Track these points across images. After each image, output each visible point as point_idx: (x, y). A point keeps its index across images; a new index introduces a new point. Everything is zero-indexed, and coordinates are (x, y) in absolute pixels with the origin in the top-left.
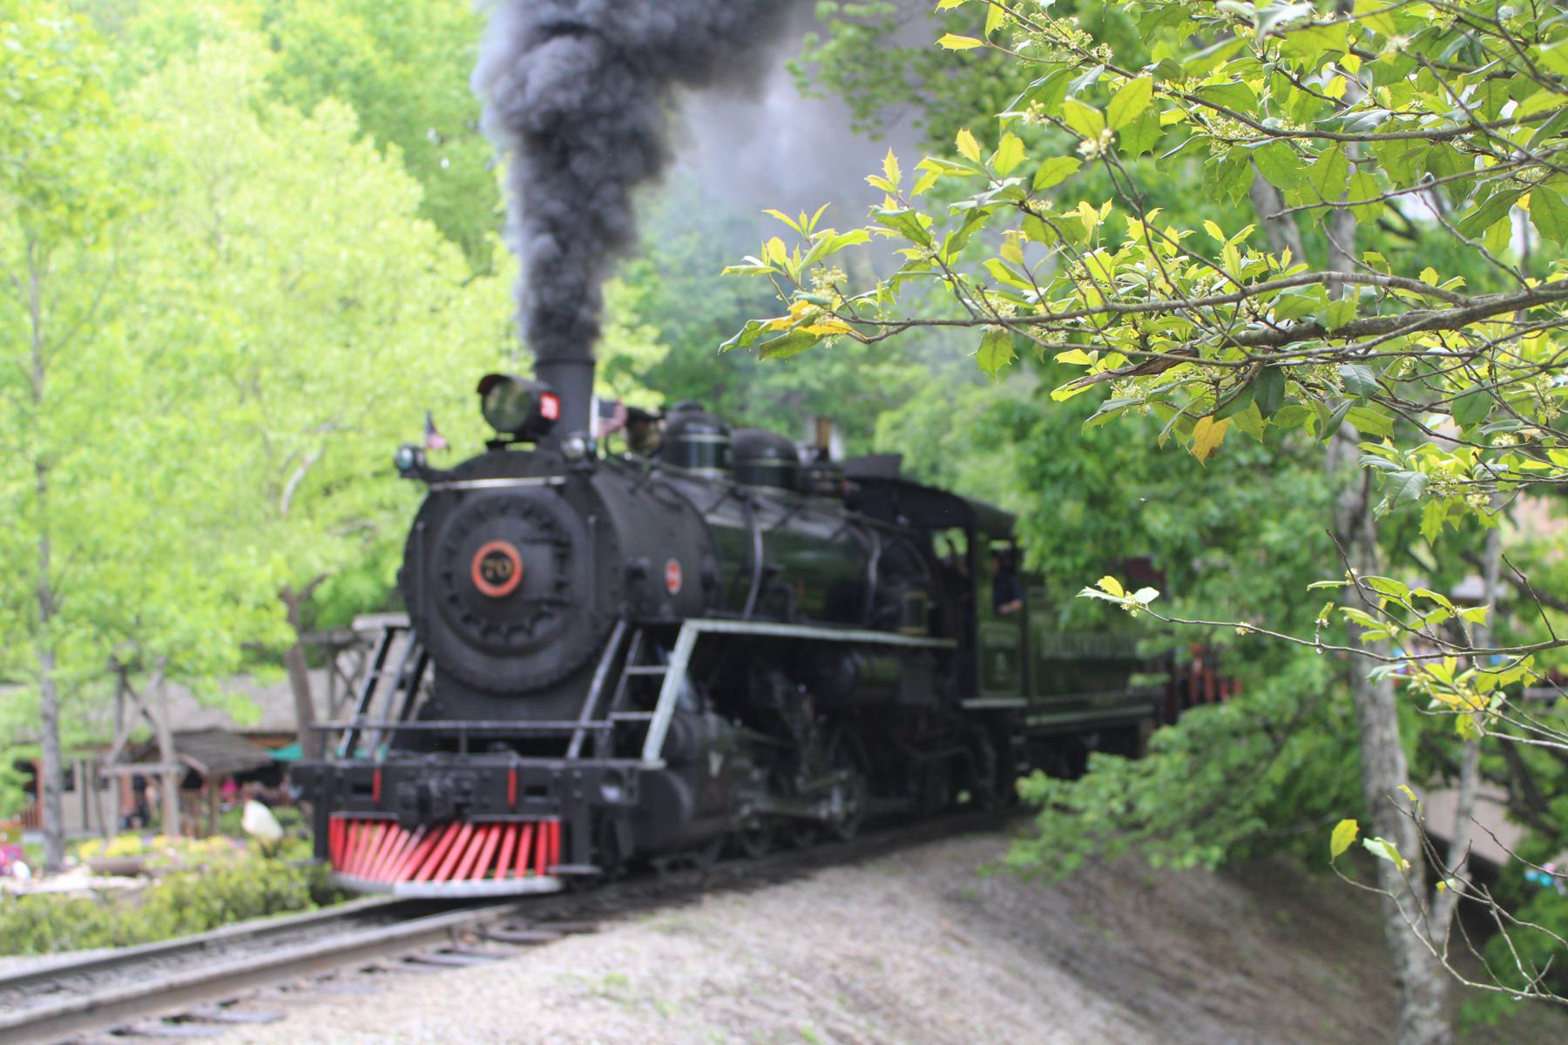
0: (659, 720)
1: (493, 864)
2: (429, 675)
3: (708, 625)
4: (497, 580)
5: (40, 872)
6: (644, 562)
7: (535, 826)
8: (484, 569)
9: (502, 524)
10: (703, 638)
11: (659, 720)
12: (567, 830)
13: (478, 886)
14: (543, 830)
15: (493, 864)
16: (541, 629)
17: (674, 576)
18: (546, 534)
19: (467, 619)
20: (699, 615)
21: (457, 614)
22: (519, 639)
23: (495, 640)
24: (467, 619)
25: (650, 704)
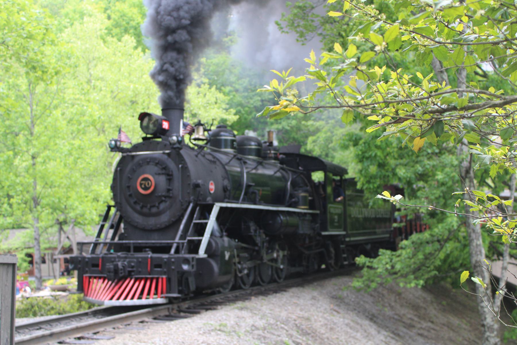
3: (224, 205)
4: (146, 189)
6: (200, 182)
7: (157, 279)
8: (141, 184)
10: (221, 208)
12: (169, 280)
14: (160, 280)
16: (162, 206)
17: (212, 187)
18: (164, 171)
19: (135, 203)
21: (132, 201)
22: (154, 210)
23: (145, 210)
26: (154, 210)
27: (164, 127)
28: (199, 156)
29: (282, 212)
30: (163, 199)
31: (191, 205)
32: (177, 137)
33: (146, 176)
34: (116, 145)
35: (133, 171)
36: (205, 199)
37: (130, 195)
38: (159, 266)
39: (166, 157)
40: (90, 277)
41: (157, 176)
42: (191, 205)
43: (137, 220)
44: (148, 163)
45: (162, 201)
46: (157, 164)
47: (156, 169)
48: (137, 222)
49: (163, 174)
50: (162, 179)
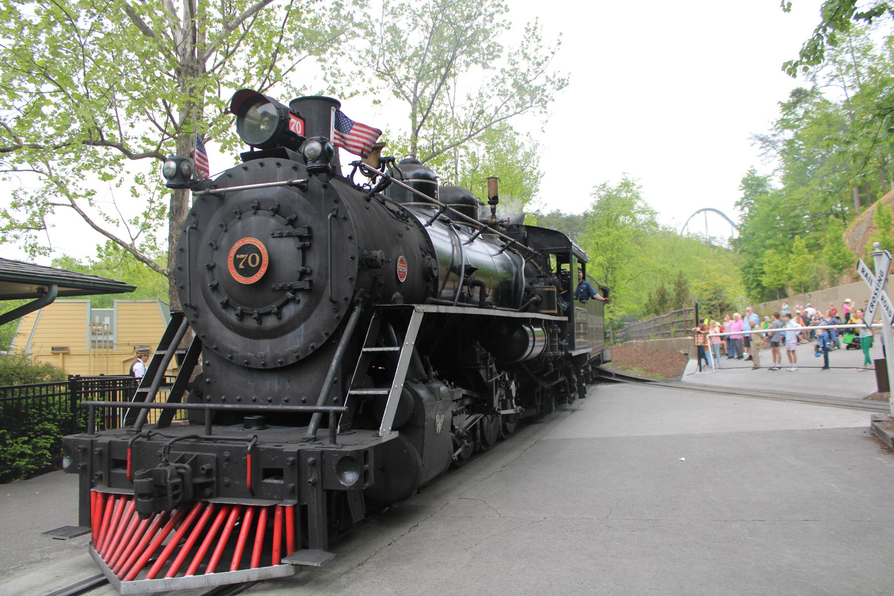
0: (394, 394)
1: (147, 565)
2: (483, 131)
3: (433, 309)
4: (248, 271)
5: (885, 394)
6: (378, 253)
7: (271, 511)
8: (237, 262)
9: (253, 220)
10: (427, 316)
11: (394, 394)
12: (301, 512)
13: (253, 573)
14: (278, 513)
15: (147, 565)
16: (290, 311)
17: (402, 269)
18: (290, 229)
19: (226, 305)
20: (423, 302)
21: (218, 300)
22: (271, 322)
23: (251, 323)
24: (226, 305)
25: (386, 380)
26: (271, 322)
27: (292, 129)
28: (373, 200)
29: (244, 189)
30: (289, 295)
31: (358, 309)
32: (323, 143)
33: (248, 241)
34: (178, 169)
35: (224, 227)
36: (387, 298)
37: (215, 288)
38: (277, 473)
39: (296, 193)
40: (106, 496)
41: (273, 242)
42: (358, 309)
43: (230, 346)
44: (257, 208)
45: (287, 302)
46: (276, 211)
47: (273, 223)
48: (232, 352)
49: (289, 235)
50: (288, 248)
